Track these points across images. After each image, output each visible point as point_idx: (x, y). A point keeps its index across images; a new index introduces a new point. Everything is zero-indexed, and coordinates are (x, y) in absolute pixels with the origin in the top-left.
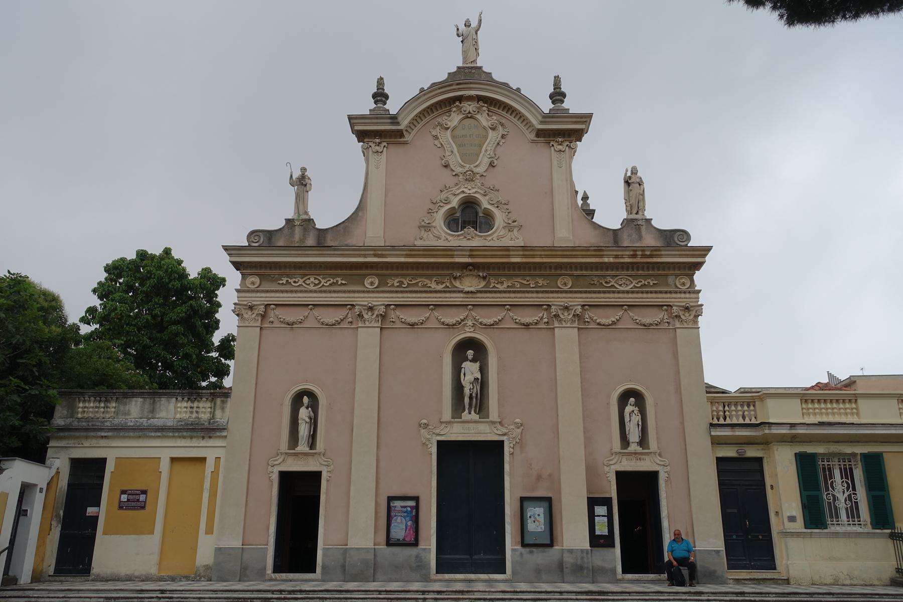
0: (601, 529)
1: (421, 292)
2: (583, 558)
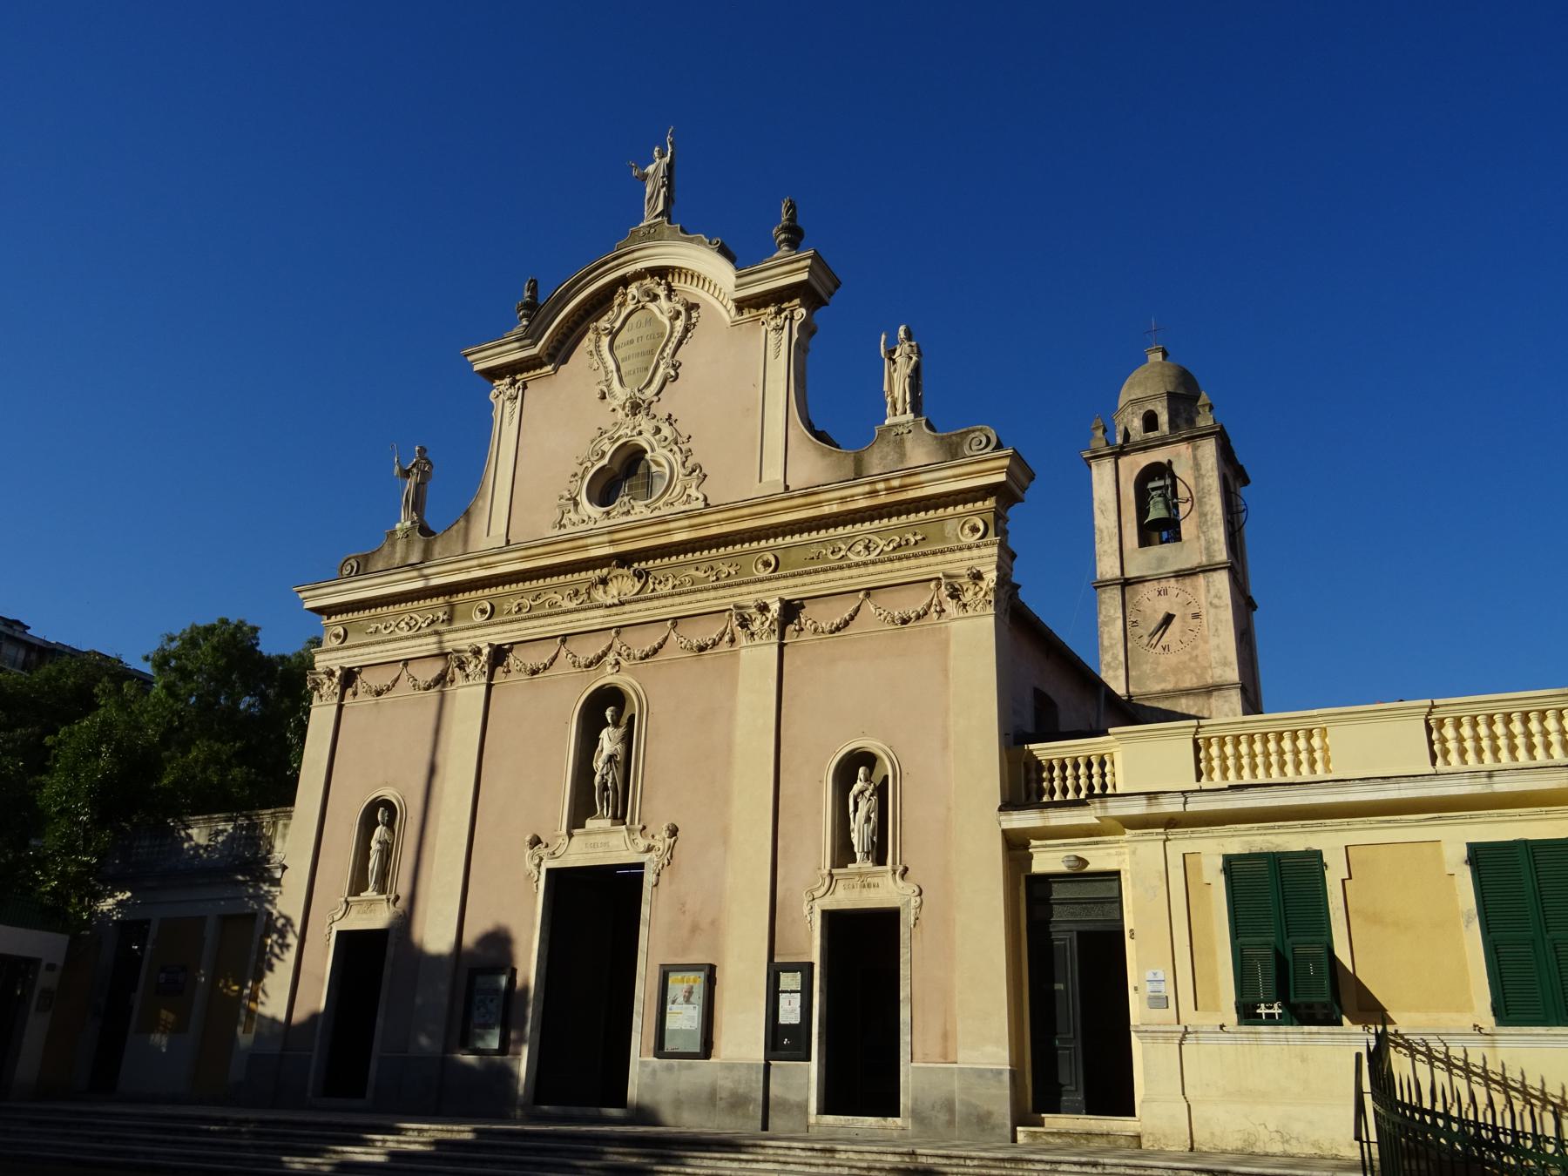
0: (790, 1012)
1: (550, 615)
2: (1053, 693)
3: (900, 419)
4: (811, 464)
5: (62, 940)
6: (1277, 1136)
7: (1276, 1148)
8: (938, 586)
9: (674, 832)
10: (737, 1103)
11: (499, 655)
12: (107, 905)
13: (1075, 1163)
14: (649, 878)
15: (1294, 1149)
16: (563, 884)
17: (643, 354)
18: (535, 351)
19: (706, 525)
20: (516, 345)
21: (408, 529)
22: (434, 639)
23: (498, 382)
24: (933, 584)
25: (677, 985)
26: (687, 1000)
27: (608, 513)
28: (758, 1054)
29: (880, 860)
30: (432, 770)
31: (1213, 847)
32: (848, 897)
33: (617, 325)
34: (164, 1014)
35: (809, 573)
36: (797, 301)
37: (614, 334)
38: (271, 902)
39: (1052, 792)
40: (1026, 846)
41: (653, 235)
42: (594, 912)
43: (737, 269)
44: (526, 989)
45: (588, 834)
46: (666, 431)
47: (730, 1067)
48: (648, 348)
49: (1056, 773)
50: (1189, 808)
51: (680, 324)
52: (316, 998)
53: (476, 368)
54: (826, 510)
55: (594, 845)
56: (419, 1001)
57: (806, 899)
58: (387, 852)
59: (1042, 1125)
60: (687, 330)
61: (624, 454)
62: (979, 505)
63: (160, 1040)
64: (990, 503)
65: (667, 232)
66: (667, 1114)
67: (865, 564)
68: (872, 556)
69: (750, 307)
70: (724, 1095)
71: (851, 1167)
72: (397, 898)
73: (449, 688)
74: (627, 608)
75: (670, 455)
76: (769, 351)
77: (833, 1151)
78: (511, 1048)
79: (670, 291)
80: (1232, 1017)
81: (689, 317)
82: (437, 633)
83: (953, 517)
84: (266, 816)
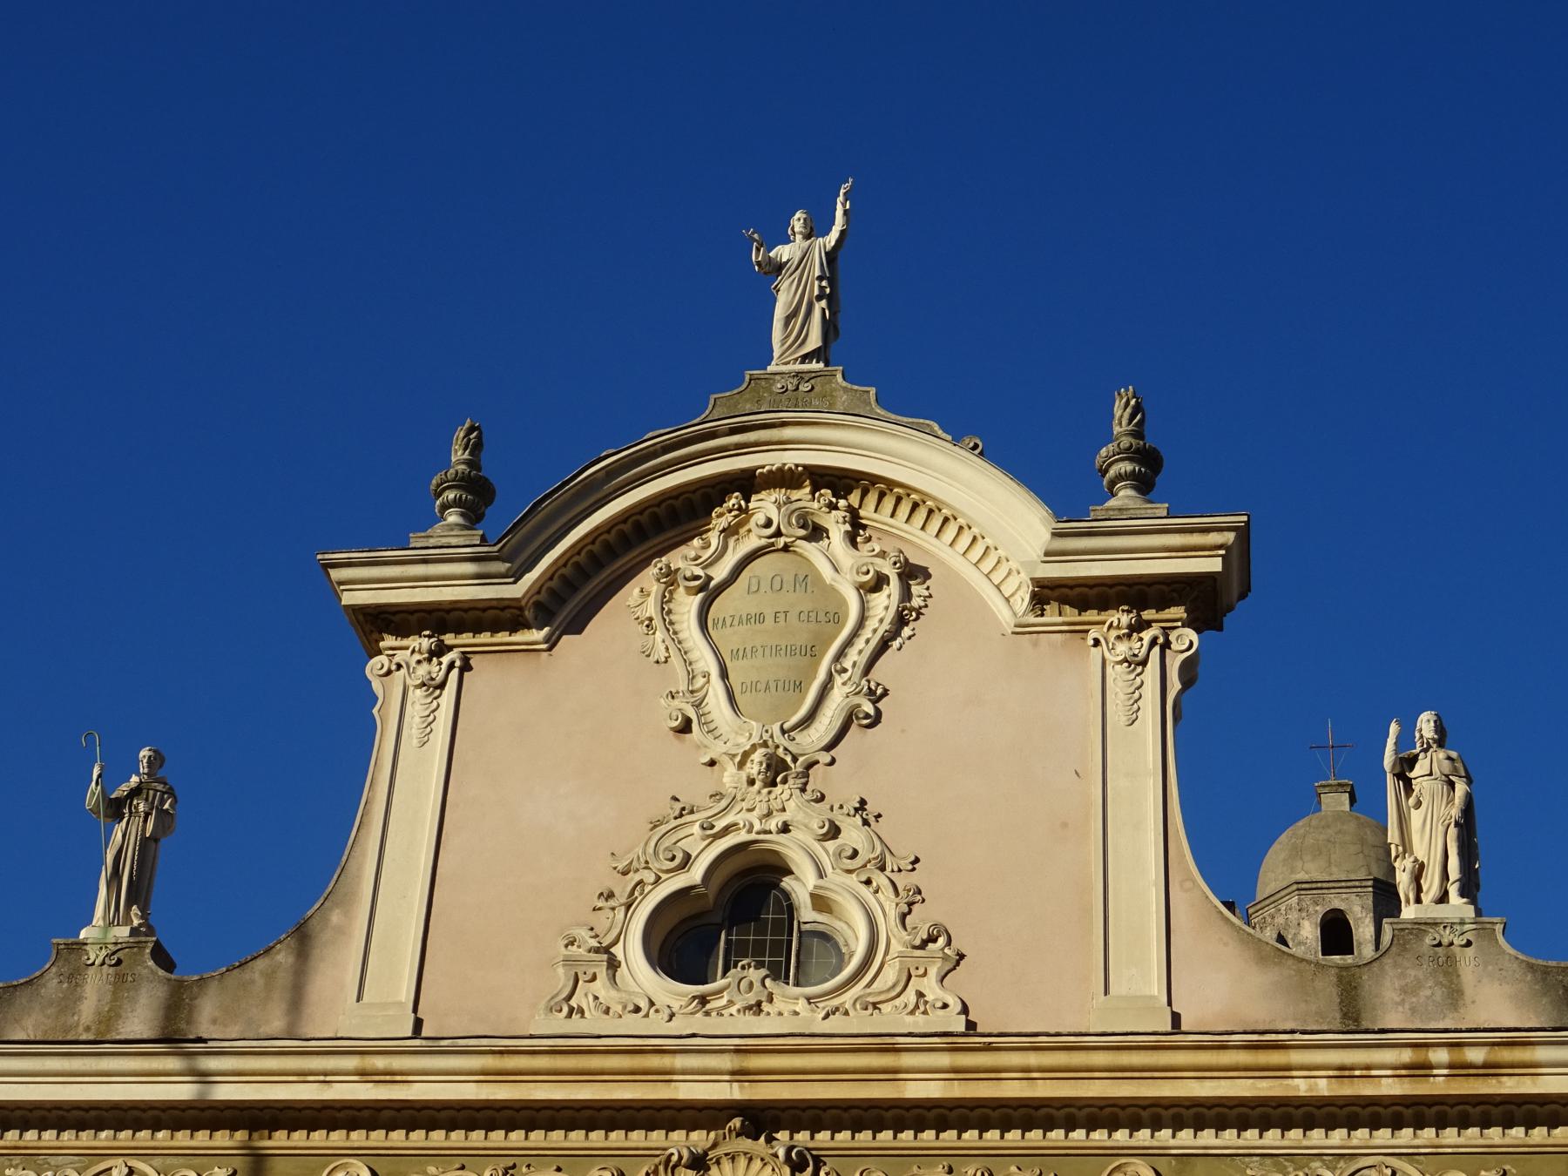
17: (791, 651)
18: (517, 591)
20: (470, 568)
21: (119, 946)
23: (389, 641)
27: (703, 1000)
33: (720, 573)
36: (1178, 612)
37: (710, 593)
41: (801, 398)
46: (853, 834)
48: (802, 638)
51: (884, 604)
53: (348, 599)
54: (1300, 1087)
60: (901, 621)
65: (842, 400)
69: (1064, 601)
75: (866, 892)
76: (1116, 709)
79: (856, 529)
81: (906, 595)
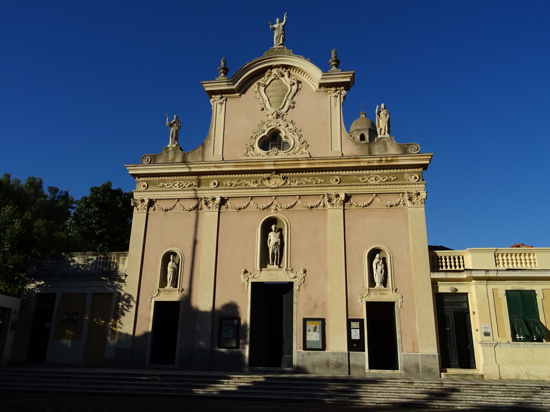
0: (355, 335)
3: (382, 136)
4: (350, 149)
5: (18, 301)
6: (526, 375)
7: (526, 378)
8: (323, 197)
9: (305, 272)
10: (338, 366)
11: (151, 203)
12: (32, 286)
13: (498, 385)
14: (296, 287)
15: (531, 378)
16: (258, 289)
18: (234, 87)
19: (314, 163)
20: (226, 83)
21: (174, 148)
22: (193, 192)
23: (213, 96)
24: (401, 195)
25: (310, 326)
26: (315, 330)
27: (268, 153)
28: (345, 349)
29: (176, 286)
30: (195, 242)
31: (502, 287)
32: (375, 297)
33: (267, 83)
34: (68, 331)
35: (354, 186)
36: (343, 88)
37: (266, 87)
38: (120, 289)
39: (442, 267)
40: (437, 284)
41: (280, 52)
42: (272, 300)
43: (323, 72)
44: (246, 325)
45: (268, 270)
46: (291, 126)
47: (335, 354)
49: (443, 260)
50: (499, 275)
51: (295, 88)
52: (146, 325)
53: (206, 89)
55: (271, 275)
56: (198, 328)
57: (359, 297)
58: (176, 272)
59: (446, 372)
60: (297, 90)
61: (273, 131)
62: (416, 170)
63: (67, 342)
64: (420, 170)
66: (310, 369)
67: (373, 185)
68: (377, 183)
69: (324, 86)
70: (333, 363)
71: (425, 388)
72: (183, 290)
73: (200, 211)
74: (280, 189)
75: (293, 135)
76: (333, 103)
77: (412, 383)
78: (241, 346)
80: (510, 339)
82: (194, 190)
83: (407, 172)
84: (114, 255)
